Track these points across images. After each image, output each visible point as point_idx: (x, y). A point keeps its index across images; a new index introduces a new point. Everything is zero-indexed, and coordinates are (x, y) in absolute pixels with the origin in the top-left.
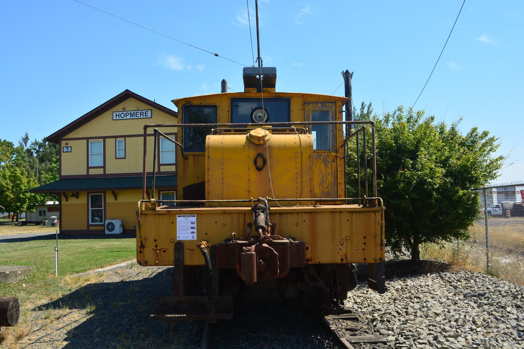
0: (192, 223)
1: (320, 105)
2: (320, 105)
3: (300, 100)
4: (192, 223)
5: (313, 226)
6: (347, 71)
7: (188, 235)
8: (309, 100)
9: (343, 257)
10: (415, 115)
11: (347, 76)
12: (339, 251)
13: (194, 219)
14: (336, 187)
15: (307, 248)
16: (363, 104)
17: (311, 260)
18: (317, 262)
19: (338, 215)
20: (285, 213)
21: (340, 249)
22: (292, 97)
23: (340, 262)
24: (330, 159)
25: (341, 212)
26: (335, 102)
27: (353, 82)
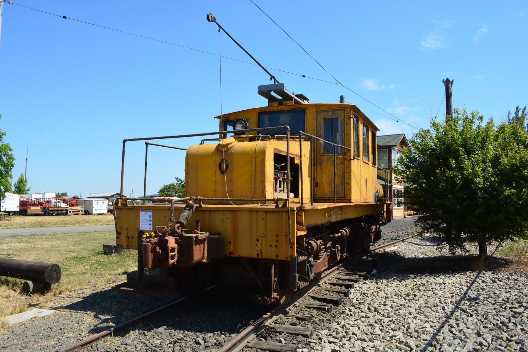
0: (150, 217)
1: (330, 113)
2: (330, 113)
3: (314, 110)
4: (150, 217)
5: (235, 223)
6: (447, 79)
7: (146, 226)
8: (321, 109)
9: (259, 252)
10: (470, 116)
11: (448, 83)
12: (256, 247)
13: (150, 213)
14: (343, 187)
15: (230, 242)
16: (517, 108)
17: (233, 253)
18: (237, 255)
19: (254, 214)
20: (213, 211)
21: (256, 245)
22: (307, 108)
23: (256, 257)
24: (338, 162)
25: (257, 211)
26: (344, 110)
27: (454, 89)
